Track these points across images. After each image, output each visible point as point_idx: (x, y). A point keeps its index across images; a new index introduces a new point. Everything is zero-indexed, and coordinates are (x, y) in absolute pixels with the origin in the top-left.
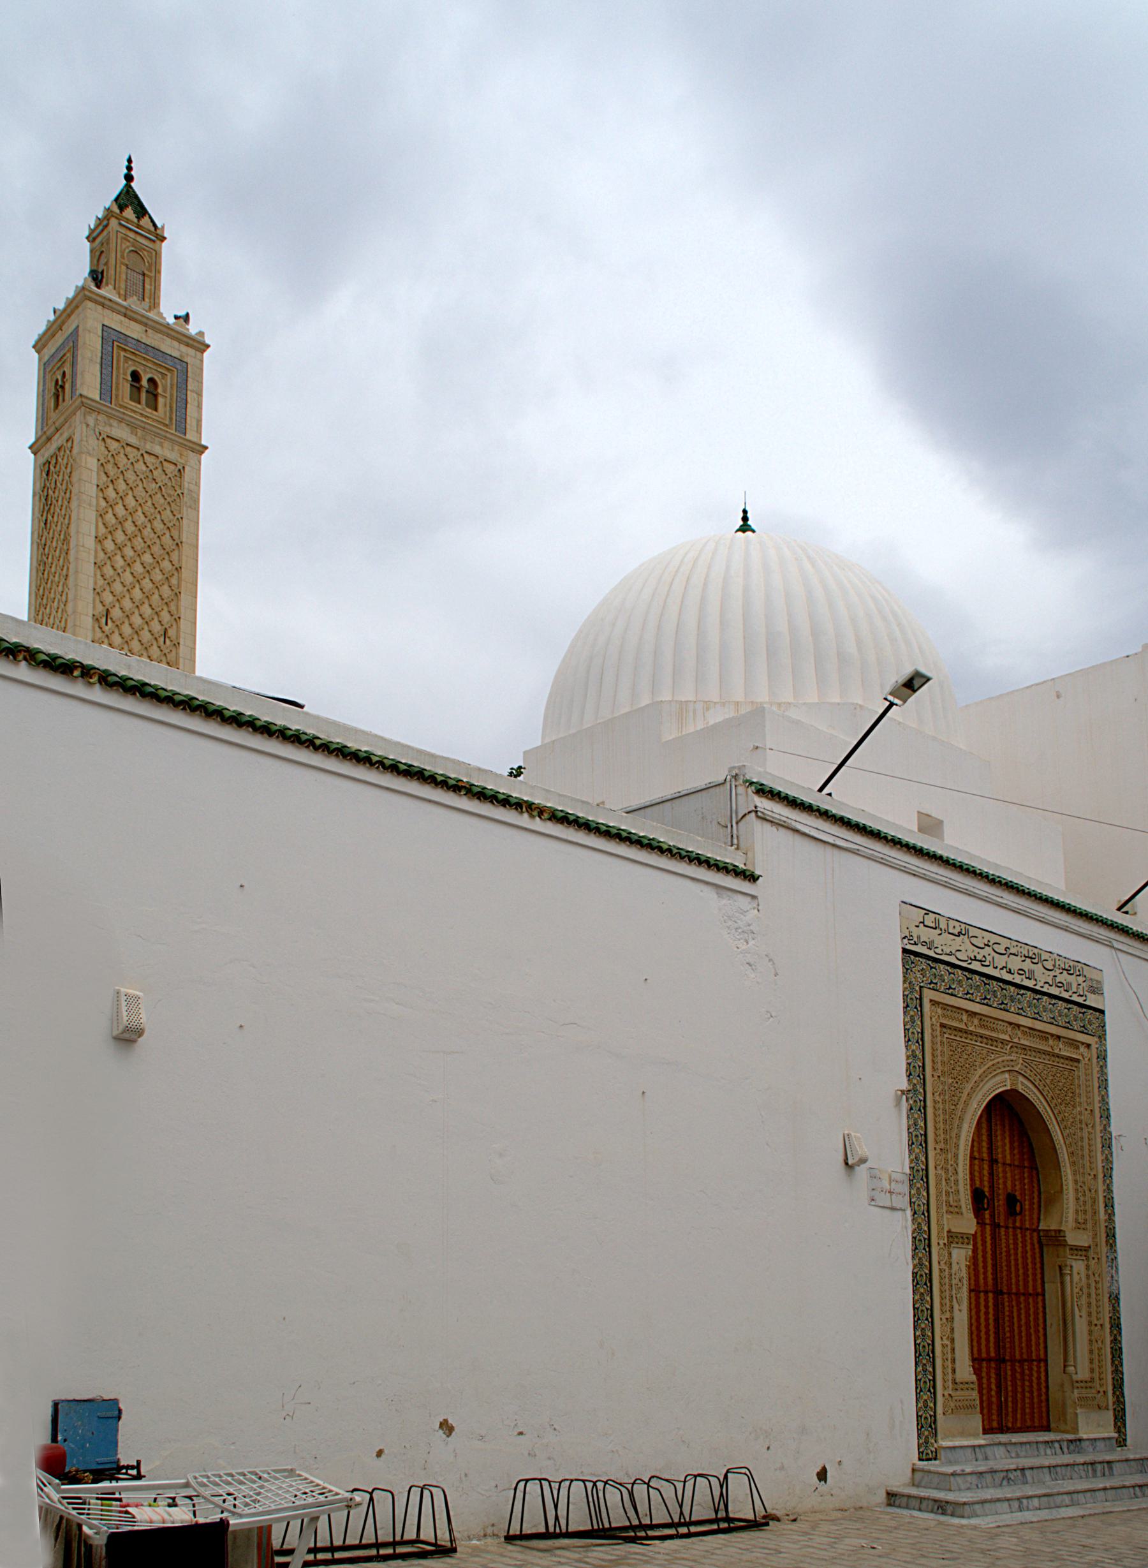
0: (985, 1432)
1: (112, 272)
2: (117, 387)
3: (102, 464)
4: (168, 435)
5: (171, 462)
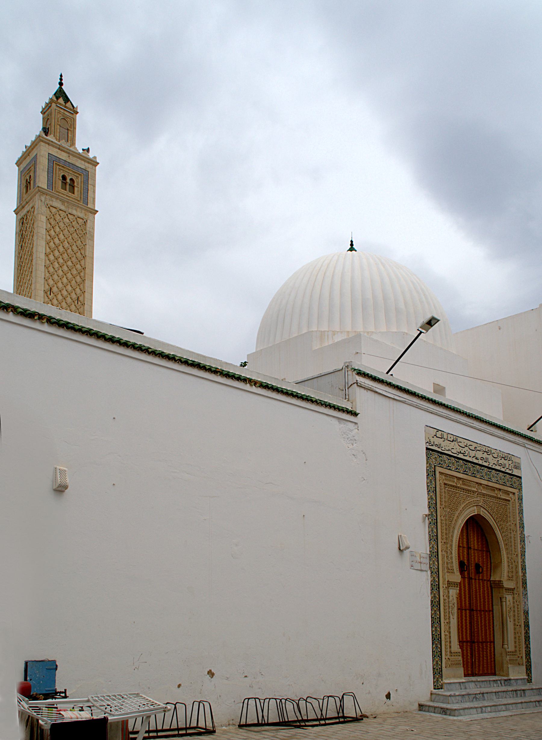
0: (465, 676)
1: (53, 128)
2: (55, 183)
3: (48, 219)
4: (79, 205)
5: (81, 218)
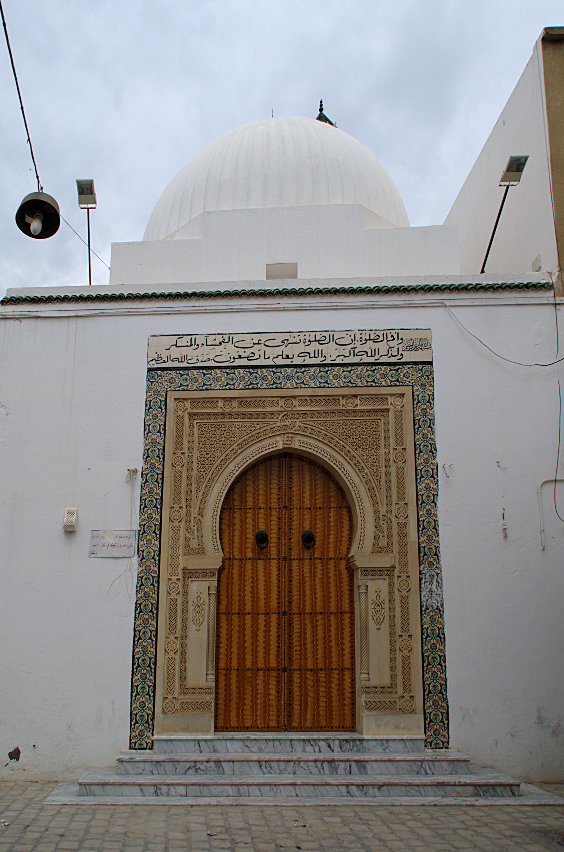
0: (217, 729)
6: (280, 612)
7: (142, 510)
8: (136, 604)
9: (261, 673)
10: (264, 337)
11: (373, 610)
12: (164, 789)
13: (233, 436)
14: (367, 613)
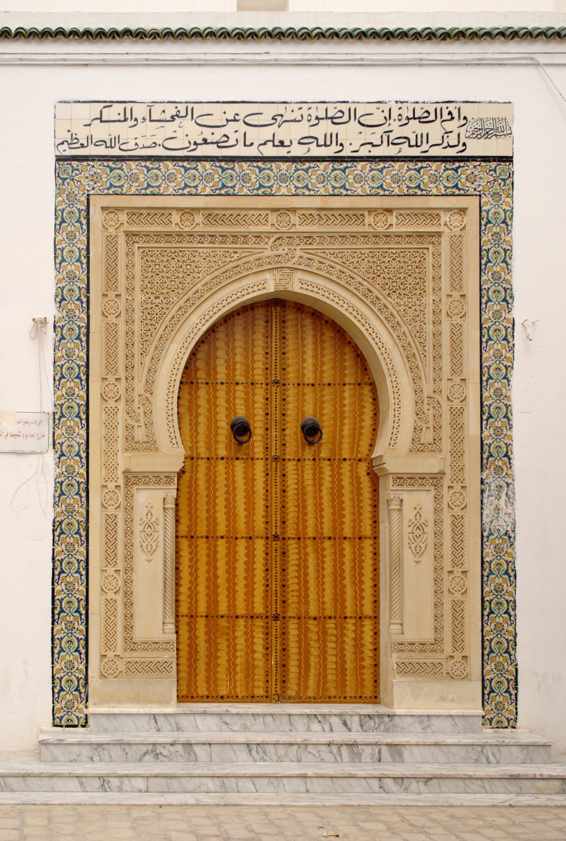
0: (181, 699)
6: (269, 535)
7: (57, 383)
8: (54, 522)
9: (241, 622)
10: (243, 110)
11: (411, 536)
12: (115, 782)
13: (196, 270)
14: (401, 538)
